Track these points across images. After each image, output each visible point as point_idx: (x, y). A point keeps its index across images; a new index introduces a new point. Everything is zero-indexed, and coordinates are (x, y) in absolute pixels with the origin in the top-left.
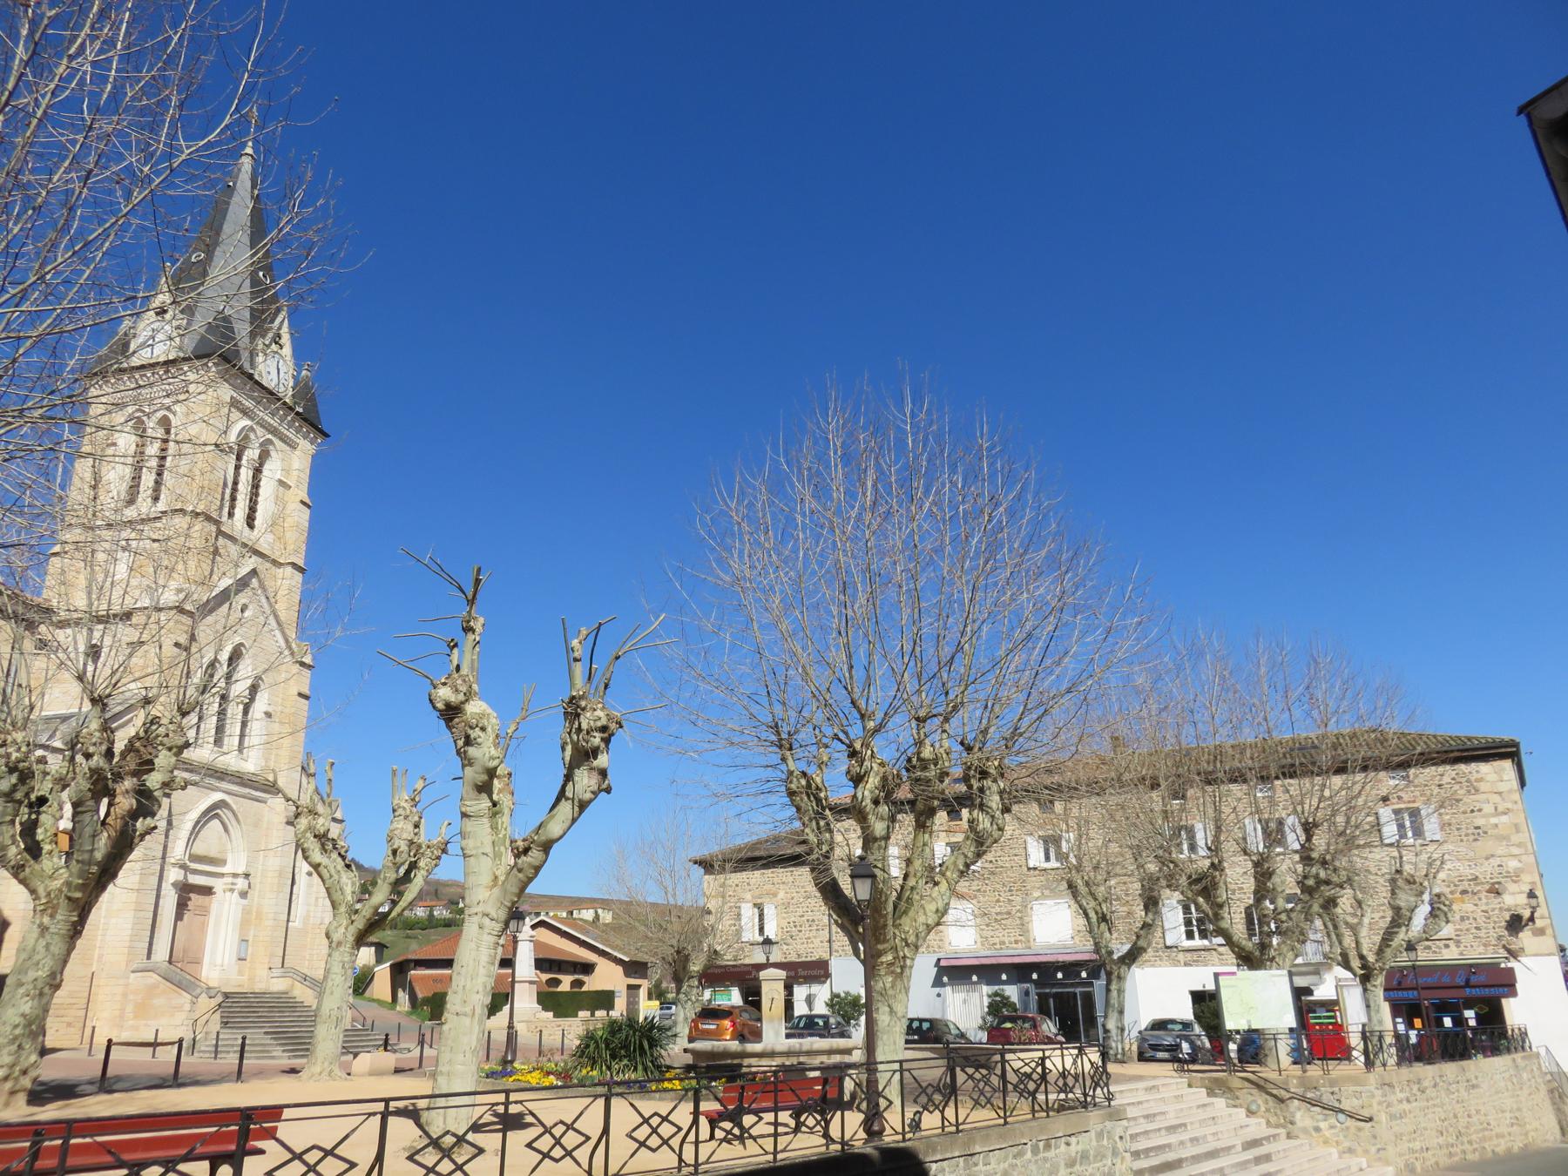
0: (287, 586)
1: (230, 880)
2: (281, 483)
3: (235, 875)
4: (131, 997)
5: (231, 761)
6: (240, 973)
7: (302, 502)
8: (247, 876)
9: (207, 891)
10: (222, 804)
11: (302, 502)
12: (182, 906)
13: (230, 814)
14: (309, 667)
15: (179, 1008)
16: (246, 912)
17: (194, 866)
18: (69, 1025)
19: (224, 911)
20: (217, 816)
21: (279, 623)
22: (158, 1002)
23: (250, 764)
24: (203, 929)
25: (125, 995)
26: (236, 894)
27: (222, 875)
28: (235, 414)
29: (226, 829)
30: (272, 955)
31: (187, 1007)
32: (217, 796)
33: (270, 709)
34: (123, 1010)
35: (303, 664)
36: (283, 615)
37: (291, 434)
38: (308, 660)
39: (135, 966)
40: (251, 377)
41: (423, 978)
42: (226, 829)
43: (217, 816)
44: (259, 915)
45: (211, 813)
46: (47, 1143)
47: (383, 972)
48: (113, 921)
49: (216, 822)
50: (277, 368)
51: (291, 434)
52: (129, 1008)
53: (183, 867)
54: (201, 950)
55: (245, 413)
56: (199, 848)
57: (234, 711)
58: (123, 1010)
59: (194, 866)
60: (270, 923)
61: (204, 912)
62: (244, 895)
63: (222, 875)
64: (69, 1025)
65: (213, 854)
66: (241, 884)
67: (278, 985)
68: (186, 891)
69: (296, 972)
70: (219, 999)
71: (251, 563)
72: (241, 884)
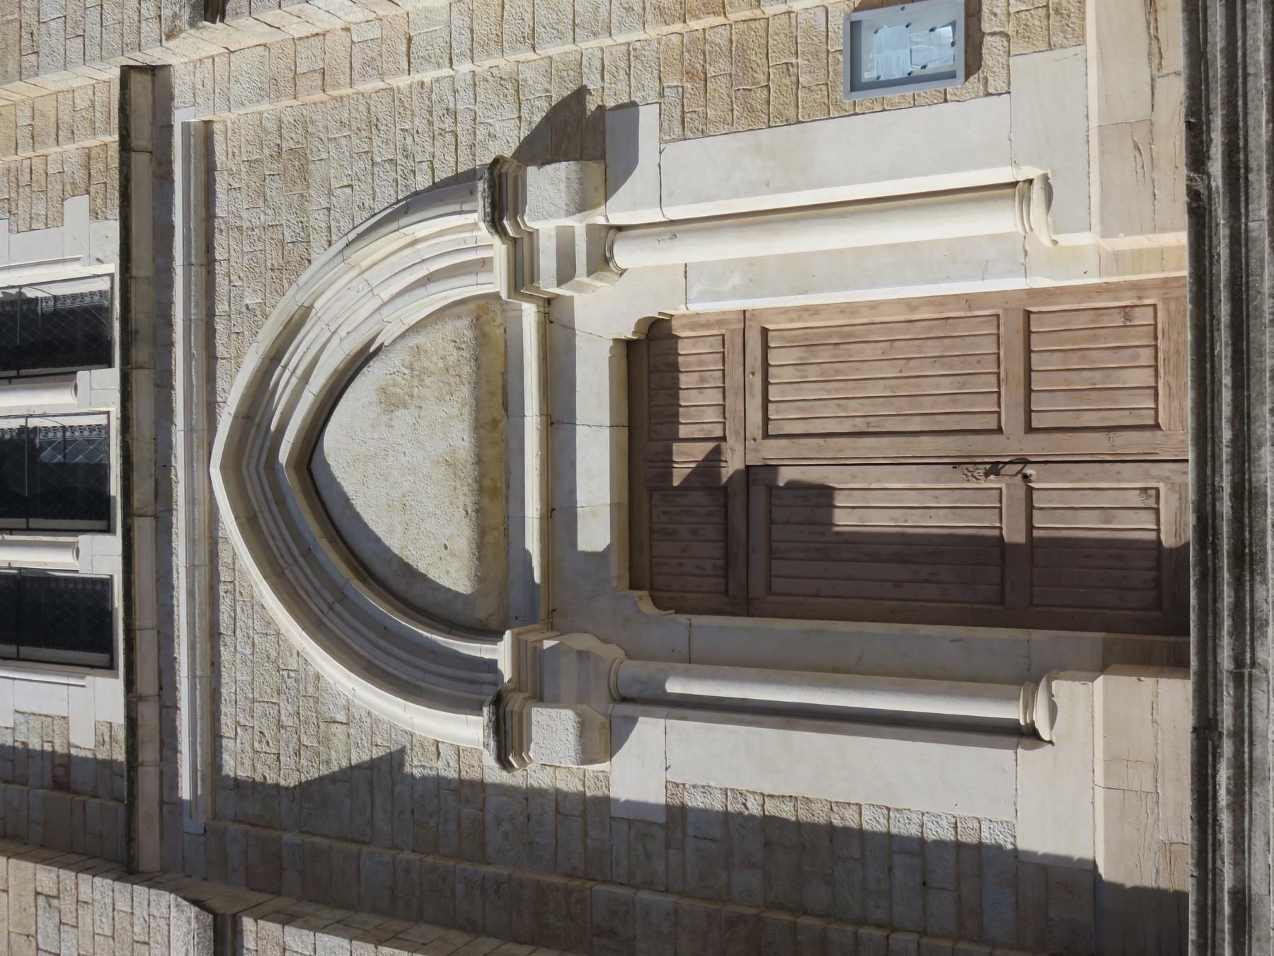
29: (363, 358)
61: (752, 342)
63: (555, 321)
69: (395, 341)
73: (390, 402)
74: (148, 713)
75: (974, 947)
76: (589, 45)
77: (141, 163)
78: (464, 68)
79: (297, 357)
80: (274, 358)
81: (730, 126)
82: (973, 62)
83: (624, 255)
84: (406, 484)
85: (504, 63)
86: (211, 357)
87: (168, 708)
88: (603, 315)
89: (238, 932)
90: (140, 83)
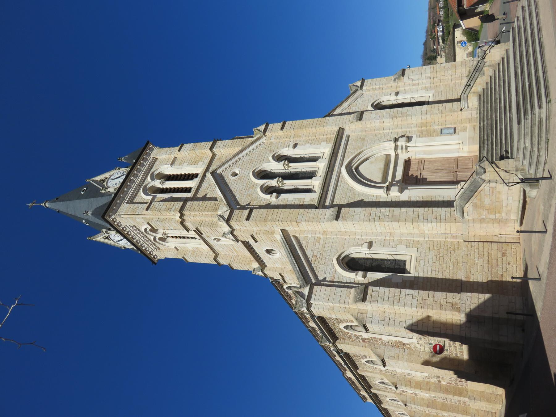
0: (225, 149)
1: (399, 151)
2: (172, 164)
3: (396, 148)
4: (483, 217)
5: (321, 166)
6: (465, 130)
7: (179, 150)
8: (396, 140)
9: (408, 163)
10: (349, 168)
11: (179, 150)
12: (419, 181)
13: (356, 159)
14: (363, 81)
15: (493, 190)
16: (421, 134)
17: (390, 179)
18: (504, 254)
19: (419, 150)
20: (357, 169)
21: (242, 151)
22: (487, 201)
23: (326, 150)
24: (433, 161)
25: (482, 221)
26: (409, 144)
27: (397, 156)
28: (137, 200)
29: (367, 159)
30: (452, 111)
31: (493, 185)
32: (343, 170)
33: (292, 145)
34: (493, 221)
35: (362, 86)
36: (237, 150)
37: (147, 164)
38: (359, 83)
39: (459, 216)
40: (116, 194)
41: (541, 246)
42: (367, 159)
43: (357, 169)
44: (423, 125)
45: (355, 174)
46: (465, 7)
47: (465, 24)
48: (427, 232)
49: (361, 168)
50: (113, 179)
51: (147, 164)
52: (492, 217)
53: (388, 189)
54: (448, 160)
55: (136, 194)
56: (377, 177)
57: (295, 167)
58: (493, 221)
59: (390, 179)
60: (428, 116)
61: (422, 162)
62: (409, 139)
63: (397, 156)
64: (504, 254)
65: (382, 165)
66: (402, 142)
67: (473, 101)
68: (409, 180)
69: (464, 92)
70: (486, 164)
71: (209, 175)
72: (402, 142)
73: (371, 163)
74: (324, 193)
75: (440, 413)
76: (408, 130)
77: (339, 137)
78: (391, 131)
79: (359, 157)
80: (355, 157)
81: (425, 137)
82: (455, 133)
83: (409, 149)
84: (373, 171)
85: (396, 130)
86: (344, 157)
87: (327, 193)
88: (403, 157)
89: (341, 209)
90: (341, 130)
